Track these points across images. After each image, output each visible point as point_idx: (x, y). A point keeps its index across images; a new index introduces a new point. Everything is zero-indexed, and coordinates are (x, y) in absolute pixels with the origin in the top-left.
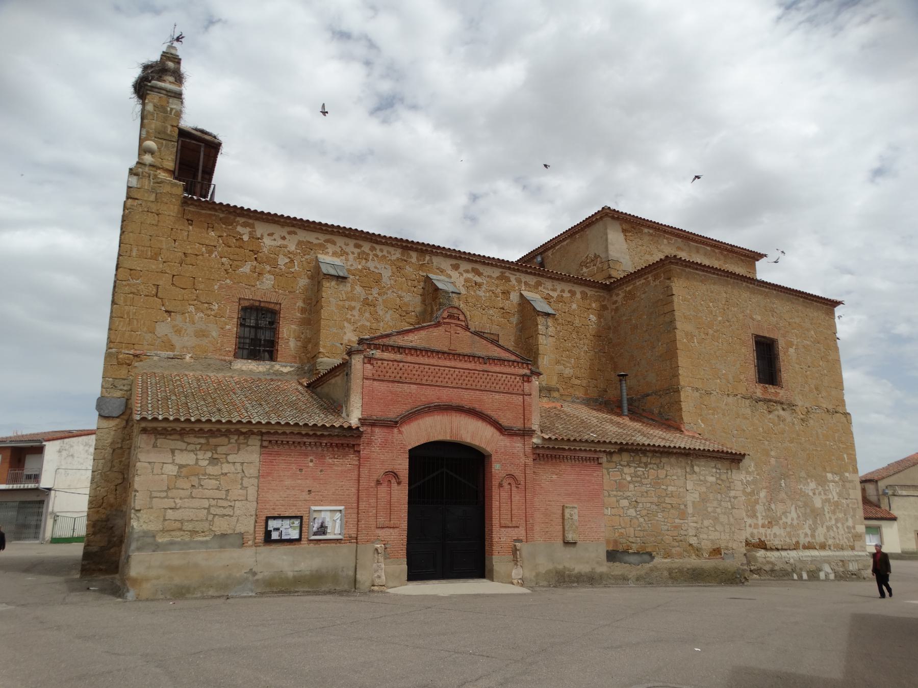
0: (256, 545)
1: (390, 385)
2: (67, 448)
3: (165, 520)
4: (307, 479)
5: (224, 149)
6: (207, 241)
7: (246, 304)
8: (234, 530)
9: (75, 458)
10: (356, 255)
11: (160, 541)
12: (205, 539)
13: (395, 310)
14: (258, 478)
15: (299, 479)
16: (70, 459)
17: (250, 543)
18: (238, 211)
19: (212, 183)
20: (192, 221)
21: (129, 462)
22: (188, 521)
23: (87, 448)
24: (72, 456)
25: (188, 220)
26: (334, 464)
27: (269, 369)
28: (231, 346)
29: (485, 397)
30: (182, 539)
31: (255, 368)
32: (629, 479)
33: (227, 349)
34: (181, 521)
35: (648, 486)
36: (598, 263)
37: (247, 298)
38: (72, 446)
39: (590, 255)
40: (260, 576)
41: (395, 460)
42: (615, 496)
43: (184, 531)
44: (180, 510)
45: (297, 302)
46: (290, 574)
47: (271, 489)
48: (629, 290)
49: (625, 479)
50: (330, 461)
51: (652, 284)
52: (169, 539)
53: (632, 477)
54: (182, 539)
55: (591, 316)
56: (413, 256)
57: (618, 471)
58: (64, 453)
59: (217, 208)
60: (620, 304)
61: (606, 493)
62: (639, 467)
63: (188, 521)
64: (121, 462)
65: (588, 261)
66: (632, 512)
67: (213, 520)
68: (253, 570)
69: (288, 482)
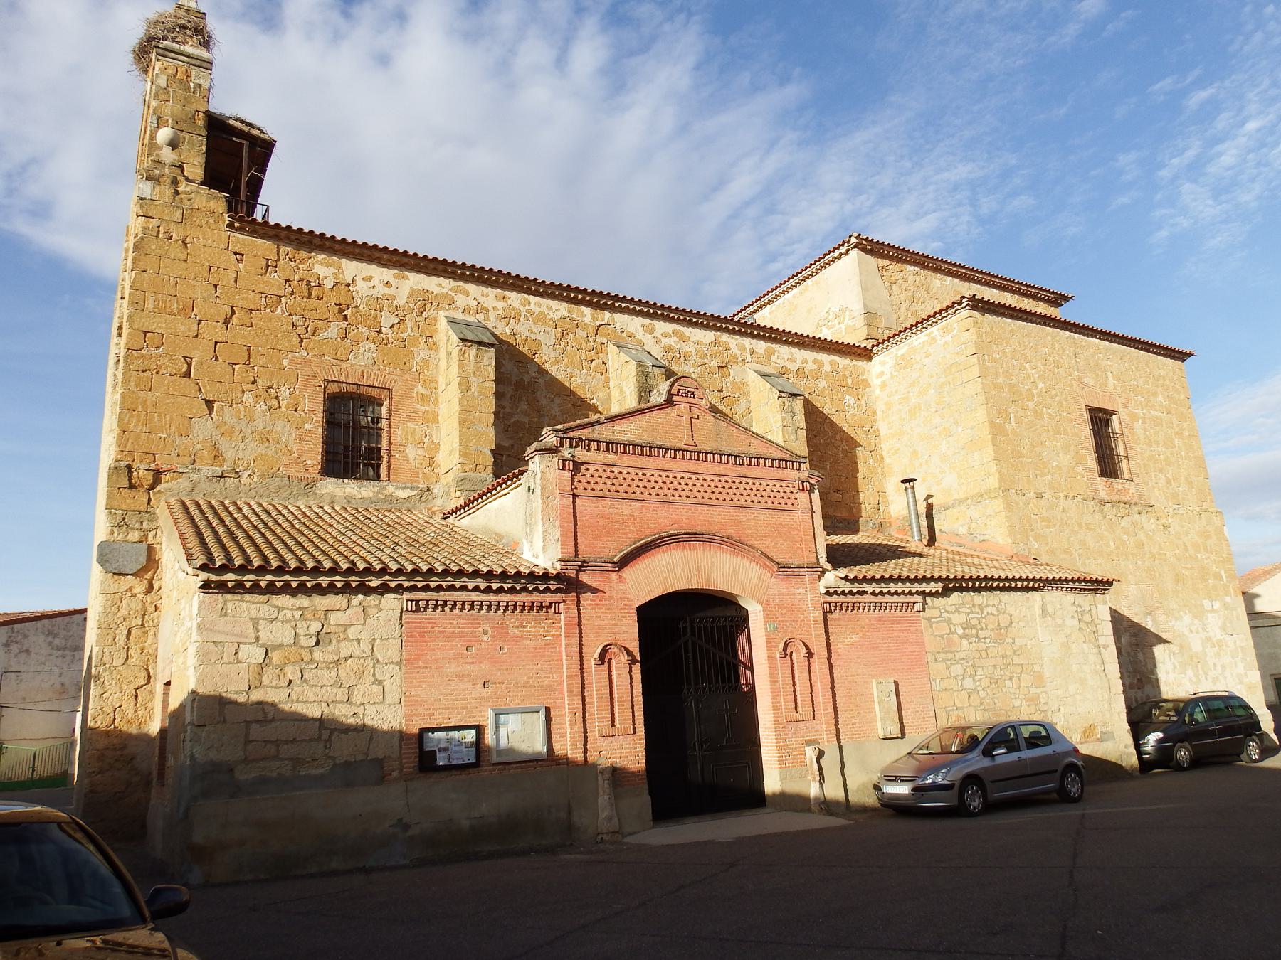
0: (408, 778)
1: (600, 503)
2: (18, 639)
3: (247, 742)
4: (481, 663)
5: (277, 145)
6: (267, 288)
7: (334, 388)
8: (367, 754)
9: (33, 655)
10: (500, 312)
11: (242, 777)
12: (320, 771)
13: (565, 397)
14: (399, 664)
15: (467, 663)
16: (23, 657)
17: (395, 774)
18: (316, 241)
19: (260, 200)
20: (242, 255)
21: (156, 649)
22: (287, 742)
23: (50, 639)
24: (28, 651)
25: (235, 253)
26: (522, 637)
27: (378, 493)
28: (313, 455)
29: (744, 519)
30: (278, 774)
31: (356, 493)
32: (960, 631)
33: (308, 462)
34: (277, 743)
35: (988, 640)
36: (847, 318)
37: (337, 379)
38: (26, 636)
39: (832, 309)
40: (414, 831)
41: (616, 624)
42: (943, 660)
43: (282, 759)
44: (273, 725)
45: (415, 386)
46: (465, 824)
47: (425, 682)
48: (902, 355)
49: (955, 633)
50: (516, 630)
51: (941, 342)
52: (258, 774)
53: (964, 629)
54: (278, 774)
55: (847, 397)
56: (585, 312)
57: (944, 621)
58: (14, 648)
59: (283, 234)
60: (889, 376)
61: (931, 658)
62: (972, 612)
63: (287, 742)
64: (142, 650)
65: (830, 317)
66: (968, 683)
67: (329, 740)
68: (404, 821)
69: (452, 668)
